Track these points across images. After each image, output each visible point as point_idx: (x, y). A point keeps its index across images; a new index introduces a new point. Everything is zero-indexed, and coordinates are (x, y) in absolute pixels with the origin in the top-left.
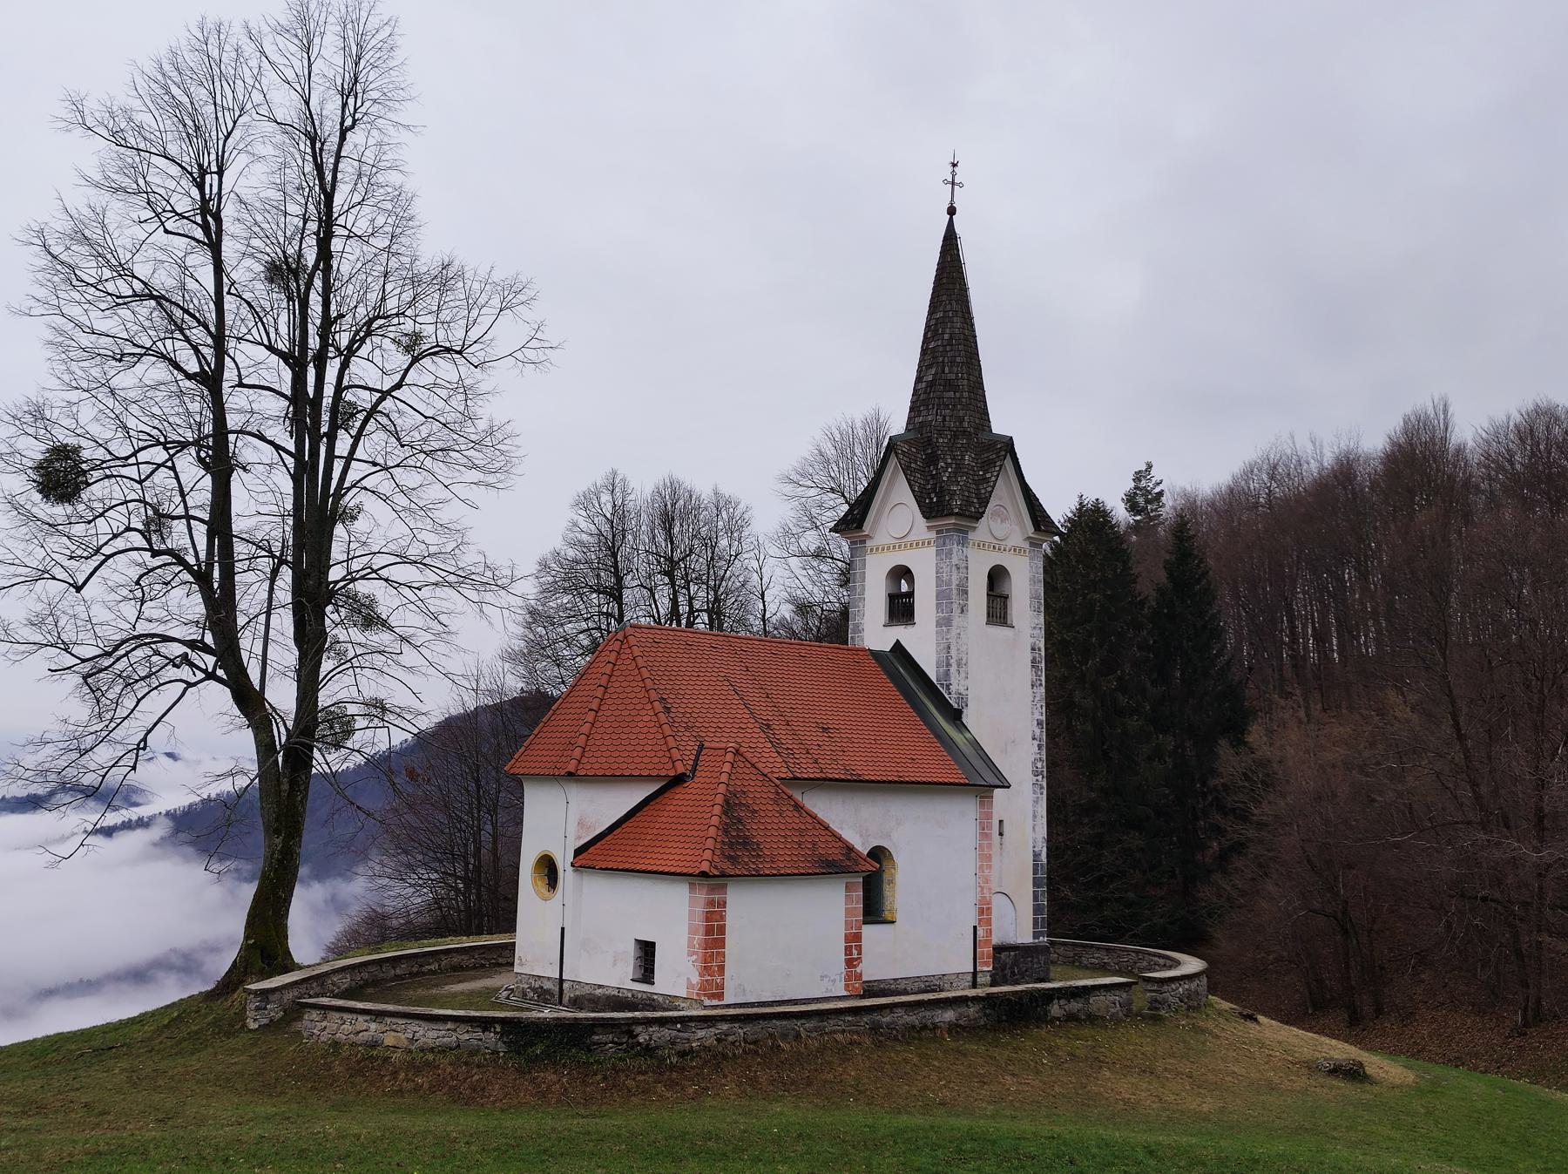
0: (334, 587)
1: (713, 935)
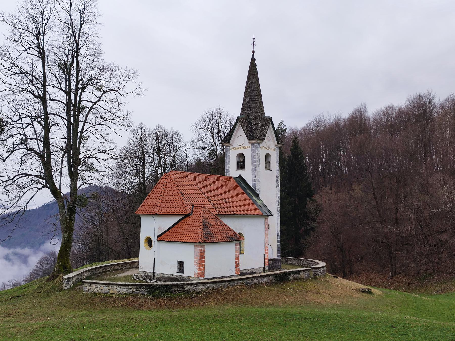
0: (81, 160)
1: (202, 259)
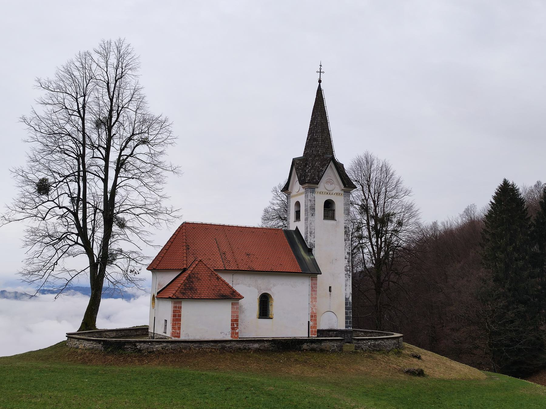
1: (177, 317)
